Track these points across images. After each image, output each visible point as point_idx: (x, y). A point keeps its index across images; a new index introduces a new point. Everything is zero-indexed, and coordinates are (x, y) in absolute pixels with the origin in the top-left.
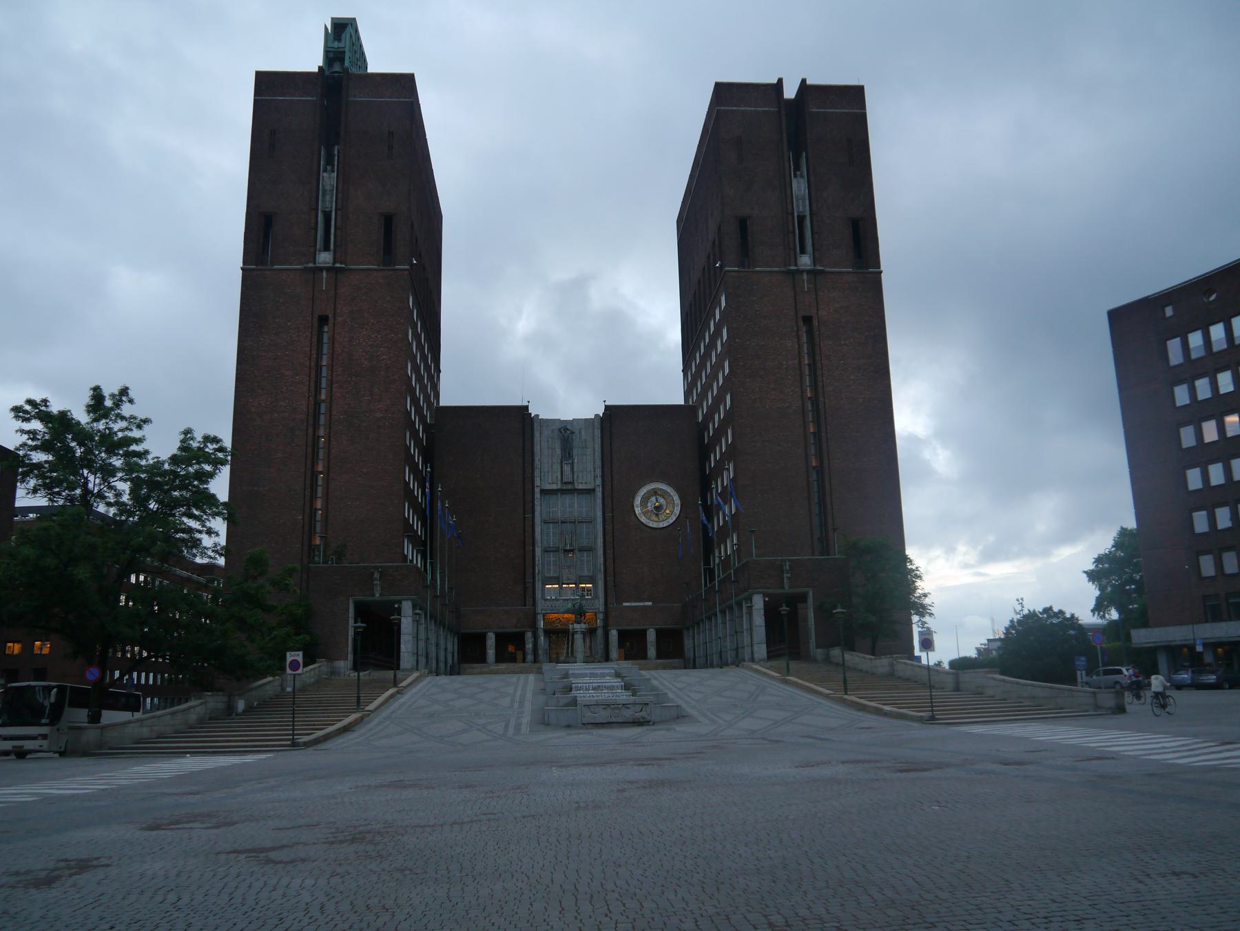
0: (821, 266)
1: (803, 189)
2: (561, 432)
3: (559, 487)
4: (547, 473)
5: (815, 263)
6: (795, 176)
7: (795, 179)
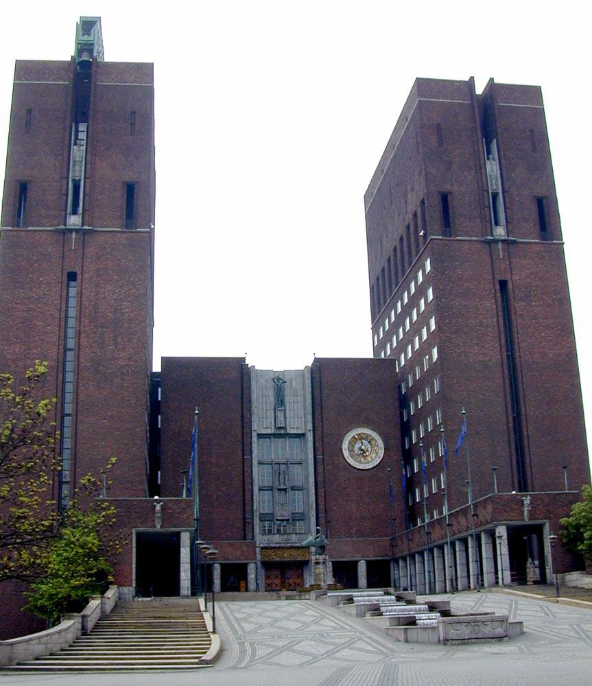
0: (513, 237)
2: (274, 382)
3: (273, 432)
4: (262, 421)
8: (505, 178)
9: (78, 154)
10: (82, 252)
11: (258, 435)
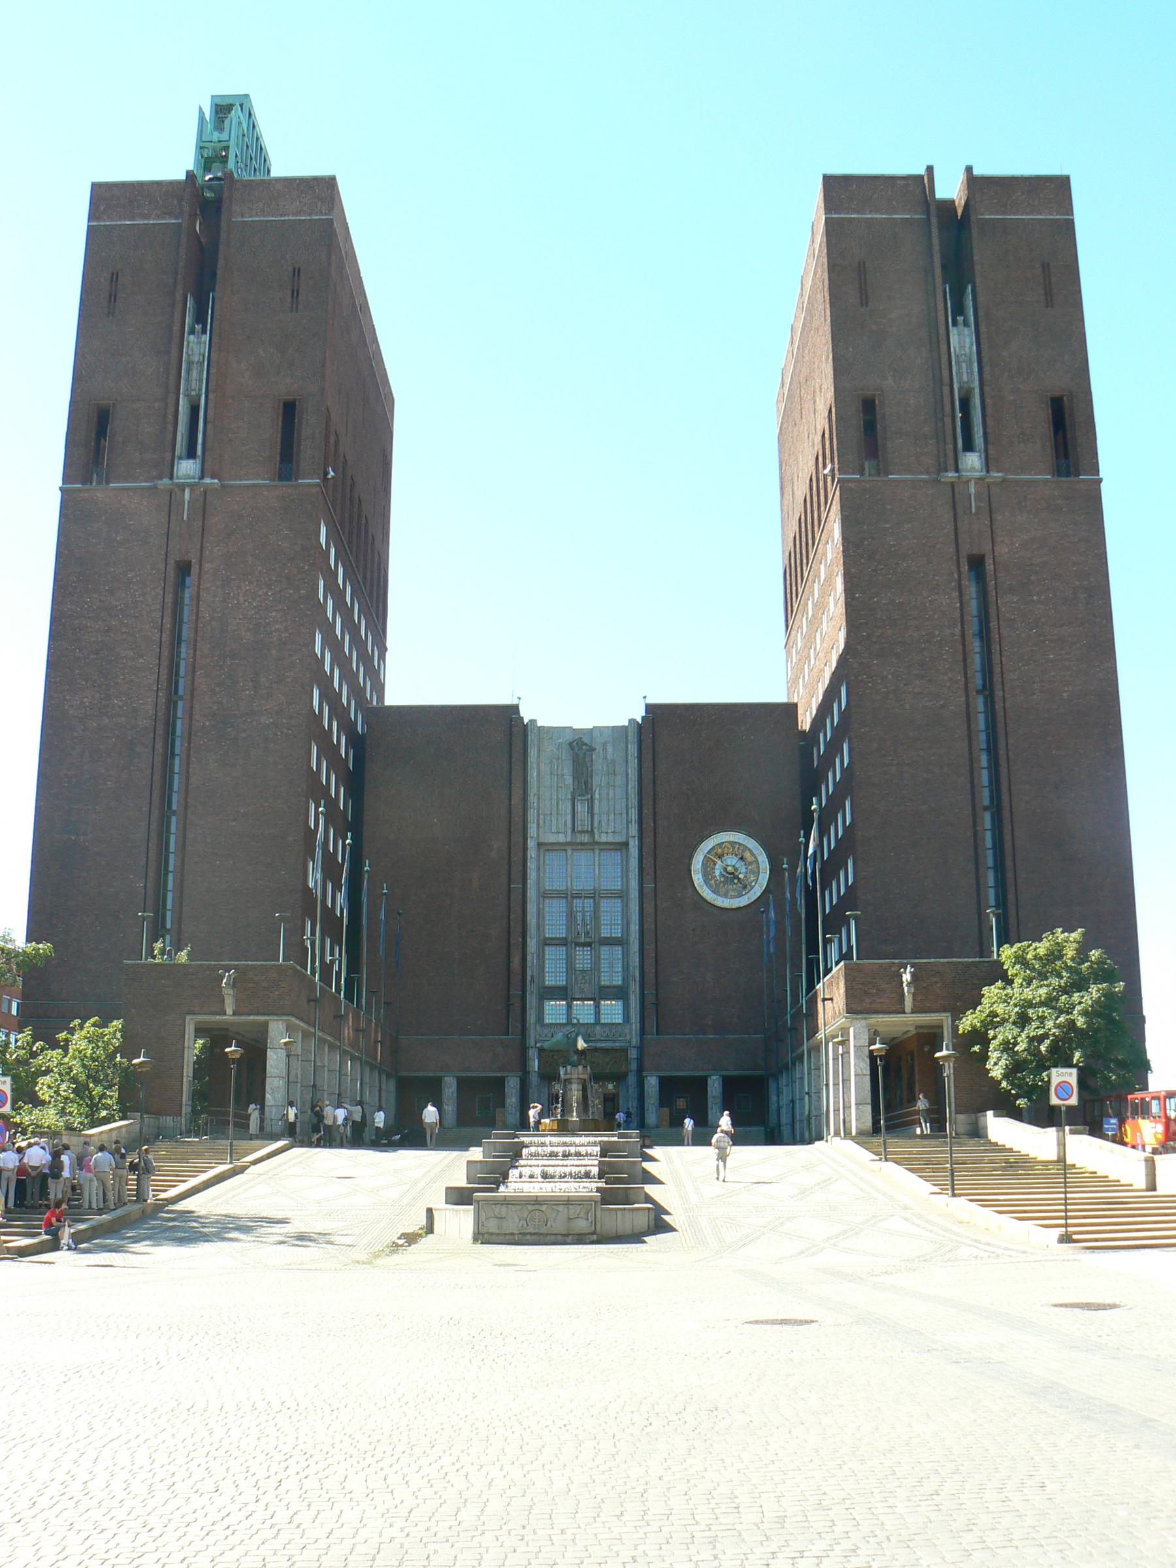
1: (968, 345)
2: (572, 749)
3: (569, 839)
5: (987, 467)
6: (955, 324)
7: (955, 328)
8: (985, 360)
9: (196, 350)
10: (200, 523)
11: (539, 845)
